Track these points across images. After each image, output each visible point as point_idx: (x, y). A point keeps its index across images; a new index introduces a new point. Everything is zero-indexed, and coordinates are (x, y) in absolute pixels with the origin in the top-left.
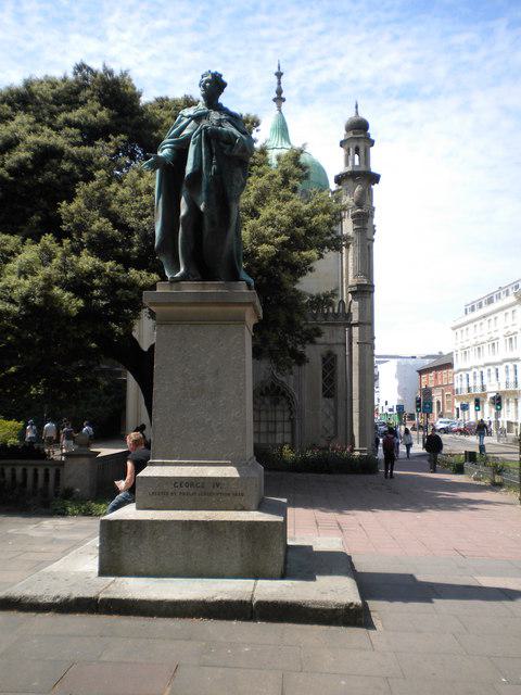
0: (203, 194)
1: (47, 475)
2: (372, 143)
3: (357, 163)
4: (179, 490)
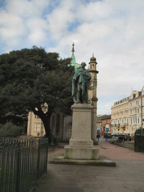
2: (97, 63)
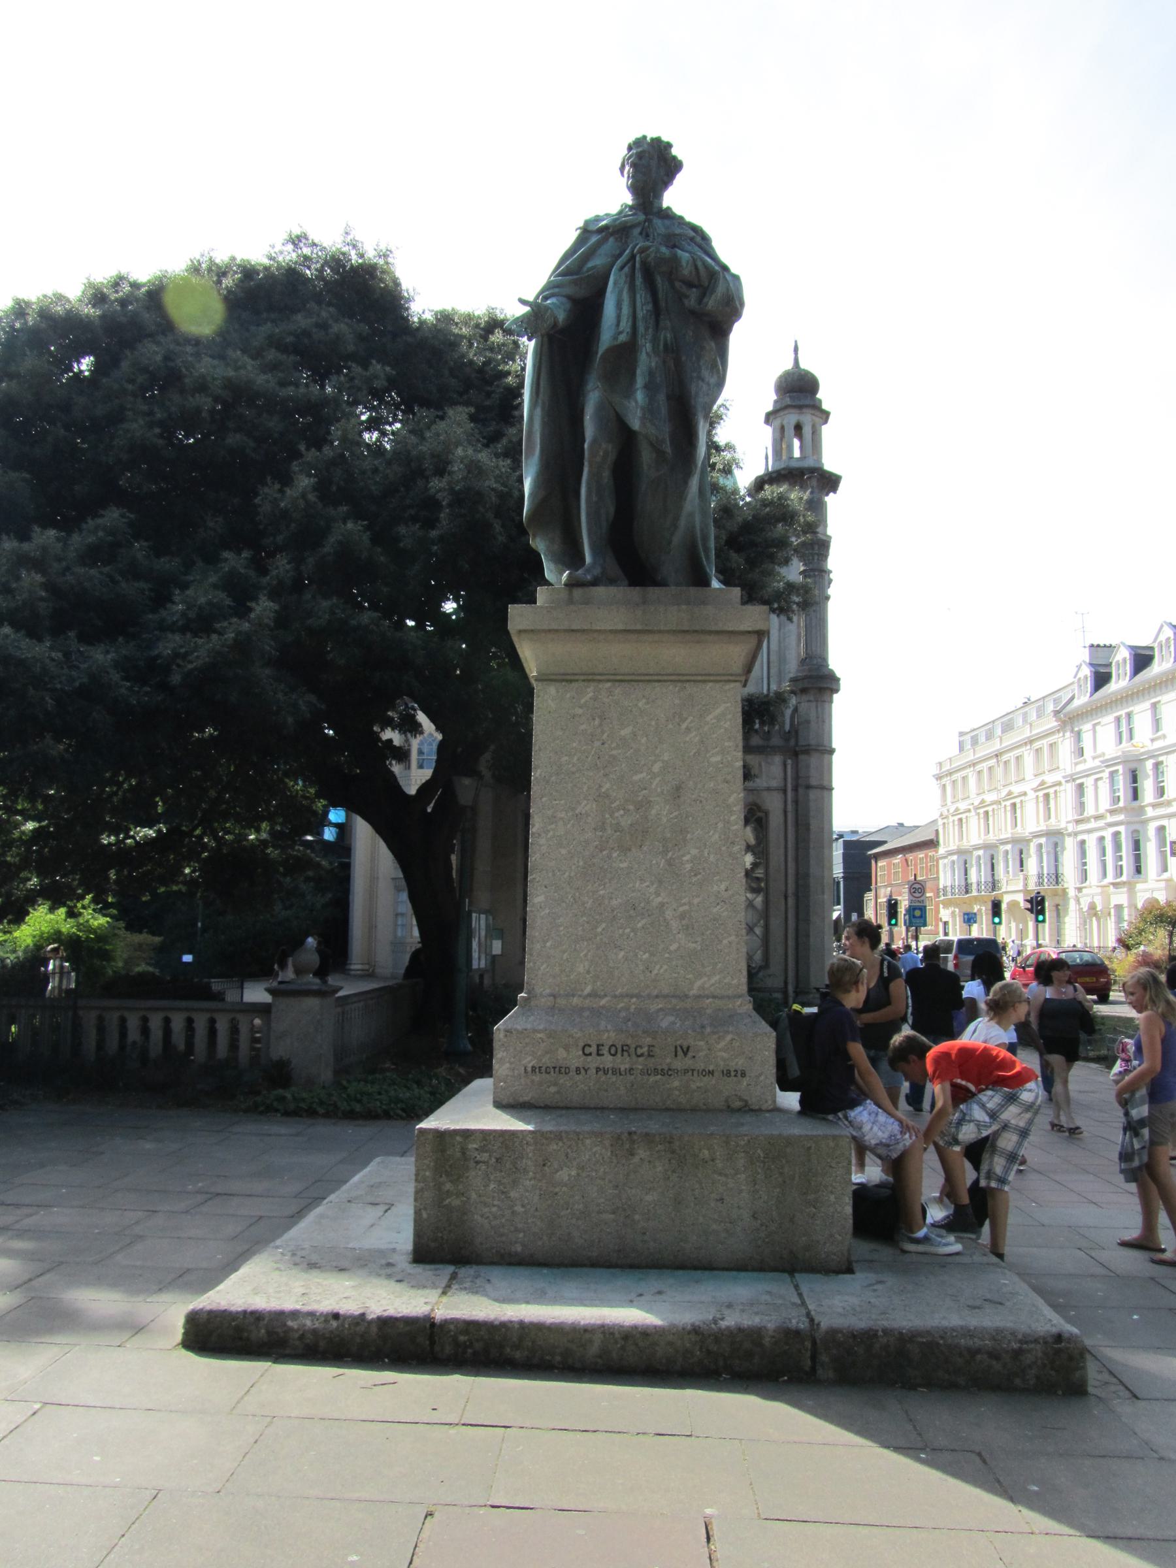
0: (640, 396)
1: (212, 1032)
3: (797, 453)
4: (593, 1062)
